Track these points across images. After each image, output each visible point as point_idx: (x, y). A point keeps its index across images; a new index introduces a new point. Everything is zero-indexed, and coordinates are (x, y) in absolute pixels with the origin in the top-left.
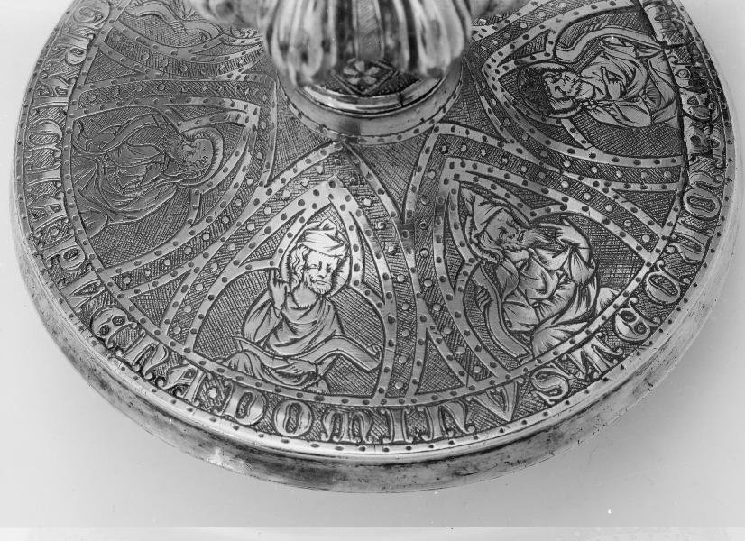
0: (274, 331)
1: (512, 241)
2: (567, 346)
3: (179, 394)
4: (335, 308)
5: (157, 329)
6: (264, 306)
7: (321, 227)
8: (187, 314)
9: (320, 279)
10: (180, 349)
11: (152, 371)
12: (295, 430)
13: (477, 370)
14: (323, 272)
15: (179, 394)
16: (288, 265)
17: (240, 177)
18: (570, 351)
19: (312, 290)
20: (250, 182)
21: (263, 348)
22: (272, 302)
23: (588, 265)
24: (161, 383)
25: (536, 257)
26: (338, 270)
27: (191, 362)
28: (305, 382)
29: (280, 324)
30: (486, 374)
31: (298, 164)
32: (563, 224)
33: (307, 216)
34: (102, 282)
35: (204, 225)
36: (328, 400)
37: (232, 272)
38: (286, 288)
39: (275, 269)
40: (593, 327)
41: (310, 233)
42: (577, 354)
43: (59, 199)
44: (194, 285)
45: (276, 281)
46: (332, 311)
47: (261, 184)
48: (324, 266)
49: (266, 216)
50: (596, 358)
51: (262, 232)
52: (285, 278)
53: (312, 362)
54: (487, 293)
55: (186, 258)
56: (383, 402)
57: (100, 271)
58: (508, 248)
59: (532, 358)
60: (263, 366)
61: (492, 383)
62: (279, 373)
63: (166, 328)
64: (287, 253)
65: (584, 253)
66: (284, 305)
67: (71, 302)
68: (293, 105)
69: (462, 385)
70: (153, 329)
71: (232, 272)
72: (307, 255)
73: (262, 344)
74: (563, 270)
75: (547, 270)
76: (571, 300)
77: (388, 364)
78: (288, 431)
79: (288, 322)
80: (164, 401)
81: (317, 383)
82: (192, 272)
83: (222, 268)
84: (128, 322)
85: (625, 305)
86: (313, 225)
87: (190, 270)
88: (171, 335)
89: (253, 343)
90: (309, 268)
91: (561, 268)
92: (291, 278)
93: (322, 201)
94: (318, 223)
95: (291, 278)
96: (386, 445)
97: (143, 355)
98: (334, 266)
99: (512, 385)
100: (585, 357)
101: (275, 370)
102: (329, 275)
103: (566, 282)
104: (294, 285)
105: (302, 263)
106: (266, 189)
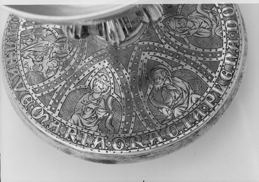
0: (205, 28)
3: (238, 45)
4: (189, 15)
5: (221, 61)
6: (199, 34)
8: (212, 55)
10: (224, 51)
11: (235, 55)
12: (231, 10)
14: (181, 22)
15: (238, 45)
16: (183, 32)
17: (163, 56)
19: (187, 23)
20: (164, 51)
21: (212, 29)
27: (226, 46)
28: (216, 14)
29: (201, 27)
33: (168, 30)
34: (214, 85)
35: (182, 63)
37: (193, 48)
38: (190, 30)
43: (192, 113)
44: (202, 57)
45: (189, 34)
46: (190, 15)
47: (164, 47)
48: (179, 22)
49: (172, 43)
51: (177, 43)
52: (187, 32)
57: (210, 87)
60: (217, 26)
63: (219, 59)
64: (180, 34)
66: (195, 29)
67: (225, 90)
71: (193, 48)
72: (178, 28)
73: (210, 29)
78: (233, 11)
79: (200, 26)
81: (214, 10)
82: (198, 59)
83: (192, 51)
84: (223, 70)
87: (198, 60)
88: (221, 56)
95: (187, 30)
101: (216, 23)
104: (188, 29)
105: (181, 29)
106: (165, 45)
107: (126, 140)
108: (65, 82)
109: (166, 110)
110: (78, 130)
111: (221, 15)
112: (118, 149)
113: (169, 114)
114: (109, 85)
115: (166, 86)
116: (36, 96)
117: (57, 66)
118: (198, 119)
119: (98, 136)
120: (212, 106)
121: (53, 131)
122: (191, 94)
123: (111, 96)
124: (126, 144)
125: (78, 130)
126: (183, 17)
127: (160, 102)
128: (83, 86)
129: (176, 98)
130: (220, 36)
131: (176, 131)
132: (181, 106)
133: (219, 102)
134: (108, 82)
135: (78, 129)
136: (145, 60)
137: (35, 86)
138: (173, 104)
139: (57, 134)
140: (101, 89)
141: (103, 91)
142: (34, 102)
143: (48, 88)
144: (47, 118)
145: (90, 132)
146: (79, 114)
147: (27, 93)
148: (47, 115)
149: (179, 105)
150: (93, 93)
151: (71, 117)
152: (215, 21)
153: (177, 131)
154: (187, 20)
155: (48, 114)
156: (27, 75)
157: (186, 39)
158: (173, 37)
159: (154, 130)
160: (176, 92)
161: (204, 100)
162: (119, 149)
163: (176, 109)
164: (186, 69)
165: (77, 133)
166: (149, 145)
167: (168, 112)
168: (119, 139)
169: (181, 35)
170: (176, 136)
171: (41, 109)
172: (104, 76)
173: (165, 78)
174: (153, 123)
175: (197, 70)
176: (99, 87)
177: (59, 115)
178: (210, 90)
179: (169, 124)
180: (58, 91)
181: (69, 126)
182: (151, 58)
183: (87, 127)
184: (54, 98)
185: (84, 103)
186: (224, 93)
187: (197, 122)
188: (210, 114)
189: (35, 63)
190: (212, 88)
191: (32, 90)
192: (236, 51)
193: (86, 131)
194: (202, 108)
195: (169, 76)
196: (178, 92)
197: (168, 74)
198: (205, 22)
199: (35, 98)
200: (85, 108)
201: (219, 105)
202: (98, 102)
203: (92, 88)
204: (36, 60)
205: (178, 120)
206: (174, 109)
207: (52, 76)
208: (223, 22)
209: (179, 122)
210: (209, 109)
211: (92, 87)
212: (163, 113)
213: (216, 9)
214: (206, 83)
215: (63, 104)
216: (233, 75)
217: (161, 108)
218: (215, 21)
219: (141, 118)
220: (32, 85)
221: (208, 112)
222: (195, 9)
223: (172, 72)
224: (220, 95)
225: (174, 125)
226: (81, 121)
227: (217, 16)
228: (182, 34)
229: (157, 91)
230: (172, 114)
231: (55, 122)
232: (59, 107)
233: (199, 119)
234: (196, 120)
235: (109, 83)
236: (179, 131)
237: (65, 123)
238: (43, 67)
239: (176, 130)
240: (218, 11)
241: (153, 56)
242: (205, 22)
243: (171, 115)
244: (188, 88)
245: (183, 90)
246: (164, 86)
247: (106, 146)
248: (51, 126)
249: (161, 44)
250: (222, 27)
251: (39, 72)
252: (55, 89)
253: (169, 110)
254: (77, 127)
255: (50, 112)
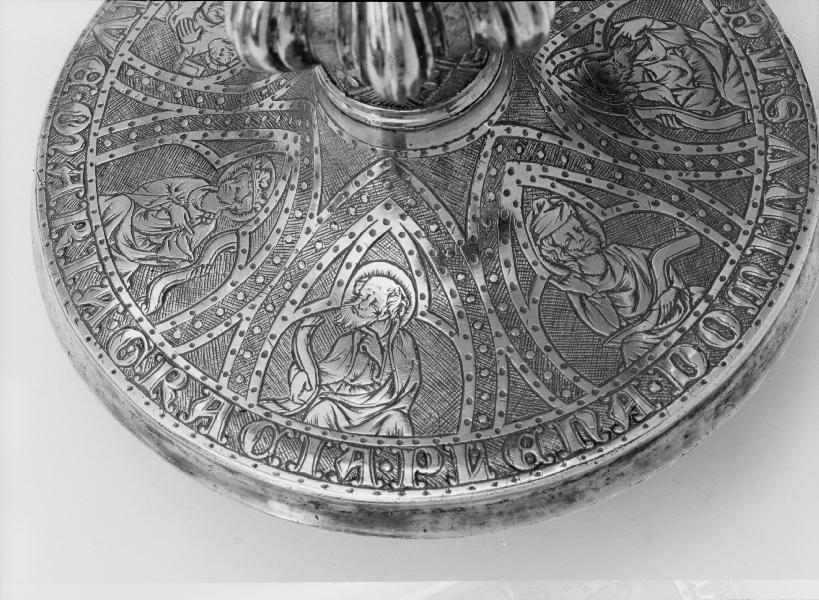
1: (620, 72)
2: (749, 80)
6: (583, 305)
7: (536, 212)
9: (583, 243)
10: (587, 400)
13: (741, 159)
14: (578, 237)
15: (639, 418)
16: (552, 264)
18: (755, 79)
22: (581, 296)
23: (671, 27)
24: (618, 430)
25: (646, 63)
26: (583, 223)
28: (685, 305)
29: (610, 298)
30: (749, 155)
31: (473, 191)
32: (619, 29)
36: (713, 292)
37: (531, 319)
39: (550, 278)
40: (738, 52)
41: (535, 227)
42: (761, 76)
48: (572, 232)
50: (772, 64)
51: (505, 270)
53: (665, 289)
54: (665, 115)
55: (490, 353)
56: (739, 247)
57: (456, 440)
58: (627, 79)
59: (749, 112)
60: (648, 332)
61: (760, 153)
62: (663, 322)
64: (541, 259)
65: (657, 25)
68: (432, 148)
69: (752, 178)
70: (552, 416)
71: (531, 319)
74: (669, 48)
75: (663, 60)
76: (701, 55)
77: (700, 227)
79: (613, 291)
80: (638, 436)
81: (691, 294)
85: (727, 20)
86: (530, 218)
88: (569, 401)
89: (618, 330)
90: (567, 247)
91: (667, 49)
92: (567, 268)
93: (516, 193)
94: (531, 212)
95: (567, 268)
96: (786, 264)
97: (579, 434)
98: (578, 224)
99: (770, 140)
100: (765, 71)
101: (657, 325)
102: (583, 233)
103: (683, 52)
107: (153, 356)
108: (195, 111)
109: (305, 385)
110: (93, 234)
111: (692, 319)
112: (115, 358)
113: (301, 398)
114: (258, 206)
115: (367, 334)
116: (112, 83)
117: (223, 65)
118: (343, 475)
119: (112, 287)
120: (408, 483)
121: (49, 187)
122: (397, 410)
123: (237, 235)
124: (142, 362)
125: (93, 234)
126: (601, 233)
127: (313, 353)
128: (213, 157)
129: (355, 383)
130: (623, 359)
131: (269, 449)
132: (346, 410)
133: (432, 488)
134: (263, 197)
135: (97, 233)
136: (381, 222)
137: (137, 63)
138: (335, 388)
139: (48, 200)
140: (236, 199)
141: (233, 208)
142: (94, 92)
143: (154, 90)
144: (72, 149)
145: (109, 264)
146: (136, 204)
147: (106, 58)
148: (81, 141)
149: (343, 404)
150: (213, 191)
151: (116, 195)
152: (659, 319)
153: (271, 451)
154: (600, 250)
155: (86, 143)
156: (153, 23)
157: (540, 285)
158: (513, 246)
159: (230, 395)
160: (373, 370)
161: (408, 450)
162: (117, 361)
163: (327, 405)
164: (453, 344)
165: (86, 238)
166: (181, 417)
167: (302, 392)
168: (141, 340)
169: (540, 266)
170: (255, 457)
171: (87, 118)
172: (268, 174)
173: (387, 316)
174: (245, 381)
175: (476, 373)
176: (238, 189)
177: (101, 169)
178: (449, 445)
179: (276, 418)
180: (162, 116)
181: (87, 208)
182: (401, 235)
183: (117, 247)
184: (136, 125)
185: (173, 191)
186: (471, 483)
187: (334, 479)
188: (382, 492)
189: (197, 16)
190: (456, 444)
191: (123, 64)
192: (615, 425)
193: (105, 254)
194: (381, 463)
195: (401, 319)
196: (376, 373)
197: (401, 314)
198: (636, 295)
199: (106, 86)
200: (160, 205)
201: (426, 494)
202: (199, 220)
203: (220, 180)
204: (206, 12)
205: (301, 433)
206: (323, 399)
207: (189, 76)
208: (676, 336)
209: (299, 439)
210: (393, 481)
211: (226, 175)
212: (290, 384)
213: (699, 295)
214: (460, 421)
215: (135, 153)
216: (537, 468)
217: (299, 368)
218: (659, 319)
219: (238, 342)
220: (134, 54)
221: (384, 484)
222: (651, 247)
223: (416, 320)
224: (456, 478)
225: (279, 432)
226: (122, 222)
227: (680, 312)
228: (544, 263)
229: (336, 325)
230: (305, 406)
231: (76, 172)
232: (119, 153)
233: (347, 476)
234: (337, 474)
235: (263, 202)
236: (273, 456)
237: (90, 195)
238: (199, 38)
239: (271, 446)
240: (697, 304)
241: (410, 234)
242: (636, 295)
243: (302, 405)
244: (406, 391)
245: (393, 381)
246: (364, 329)
247: (100, 327)
248: (57, 173)
249: (460, 228)
250: (656, 345)
251: (181, 42)
252: (161, 107)
253: (311, 389)
254: (97, 227)
255: (93, 144)
